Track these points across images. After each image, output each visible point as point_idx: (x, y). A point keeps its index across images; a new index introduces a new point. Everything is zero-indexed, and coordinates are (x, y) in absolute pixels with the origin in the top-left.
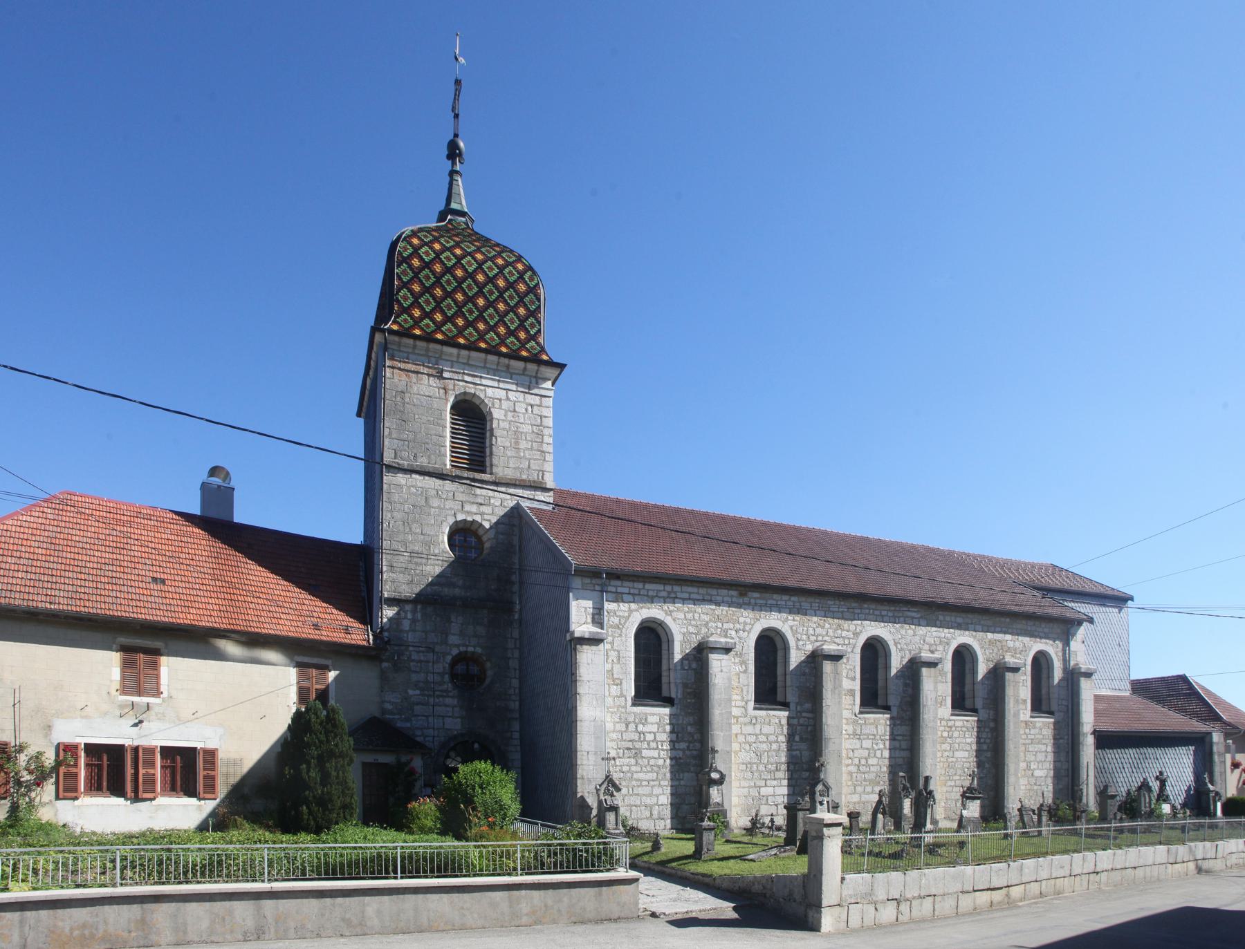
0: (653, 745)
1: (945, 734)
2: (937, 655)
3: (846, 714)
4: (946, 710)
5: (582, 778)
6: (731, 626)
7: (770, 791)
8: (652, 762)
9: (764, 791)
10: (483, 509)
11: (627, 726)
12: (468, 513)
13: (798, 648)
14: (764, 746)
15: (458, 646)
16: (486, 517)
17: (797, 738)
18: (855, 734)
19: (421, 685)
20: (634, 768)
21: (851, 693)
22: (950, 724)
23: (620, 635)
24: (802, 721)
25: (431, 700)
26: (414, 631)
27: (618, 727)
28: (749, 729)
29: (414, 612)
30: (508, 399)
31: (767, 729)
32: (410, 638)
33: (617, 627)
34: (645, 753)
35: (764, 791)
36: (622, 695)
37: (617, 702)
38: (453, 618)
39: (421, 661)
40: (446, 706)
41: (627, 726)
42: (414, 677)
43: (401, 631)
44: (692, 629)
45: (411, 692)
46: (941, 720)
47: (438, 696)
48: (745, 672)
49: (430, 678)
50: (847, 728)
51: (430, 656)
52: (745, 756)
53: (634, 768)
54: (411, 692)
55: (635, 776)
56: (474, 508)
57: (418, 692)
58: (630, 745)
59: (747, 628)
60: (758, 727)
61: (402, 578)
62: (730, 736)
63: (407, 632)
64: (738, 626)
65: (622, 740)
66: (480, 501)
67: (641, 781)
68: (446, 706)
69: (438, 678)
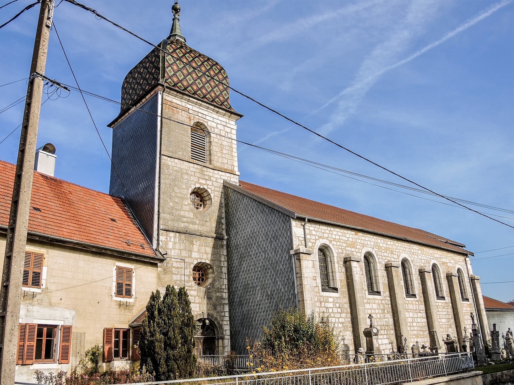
12: (201, 184)
15: (197, 259)
17: (386, 312)
26: (175, 249)
29: (175, 237)
38: (194, 242)
43: (168, 249)
56: (203, 182)
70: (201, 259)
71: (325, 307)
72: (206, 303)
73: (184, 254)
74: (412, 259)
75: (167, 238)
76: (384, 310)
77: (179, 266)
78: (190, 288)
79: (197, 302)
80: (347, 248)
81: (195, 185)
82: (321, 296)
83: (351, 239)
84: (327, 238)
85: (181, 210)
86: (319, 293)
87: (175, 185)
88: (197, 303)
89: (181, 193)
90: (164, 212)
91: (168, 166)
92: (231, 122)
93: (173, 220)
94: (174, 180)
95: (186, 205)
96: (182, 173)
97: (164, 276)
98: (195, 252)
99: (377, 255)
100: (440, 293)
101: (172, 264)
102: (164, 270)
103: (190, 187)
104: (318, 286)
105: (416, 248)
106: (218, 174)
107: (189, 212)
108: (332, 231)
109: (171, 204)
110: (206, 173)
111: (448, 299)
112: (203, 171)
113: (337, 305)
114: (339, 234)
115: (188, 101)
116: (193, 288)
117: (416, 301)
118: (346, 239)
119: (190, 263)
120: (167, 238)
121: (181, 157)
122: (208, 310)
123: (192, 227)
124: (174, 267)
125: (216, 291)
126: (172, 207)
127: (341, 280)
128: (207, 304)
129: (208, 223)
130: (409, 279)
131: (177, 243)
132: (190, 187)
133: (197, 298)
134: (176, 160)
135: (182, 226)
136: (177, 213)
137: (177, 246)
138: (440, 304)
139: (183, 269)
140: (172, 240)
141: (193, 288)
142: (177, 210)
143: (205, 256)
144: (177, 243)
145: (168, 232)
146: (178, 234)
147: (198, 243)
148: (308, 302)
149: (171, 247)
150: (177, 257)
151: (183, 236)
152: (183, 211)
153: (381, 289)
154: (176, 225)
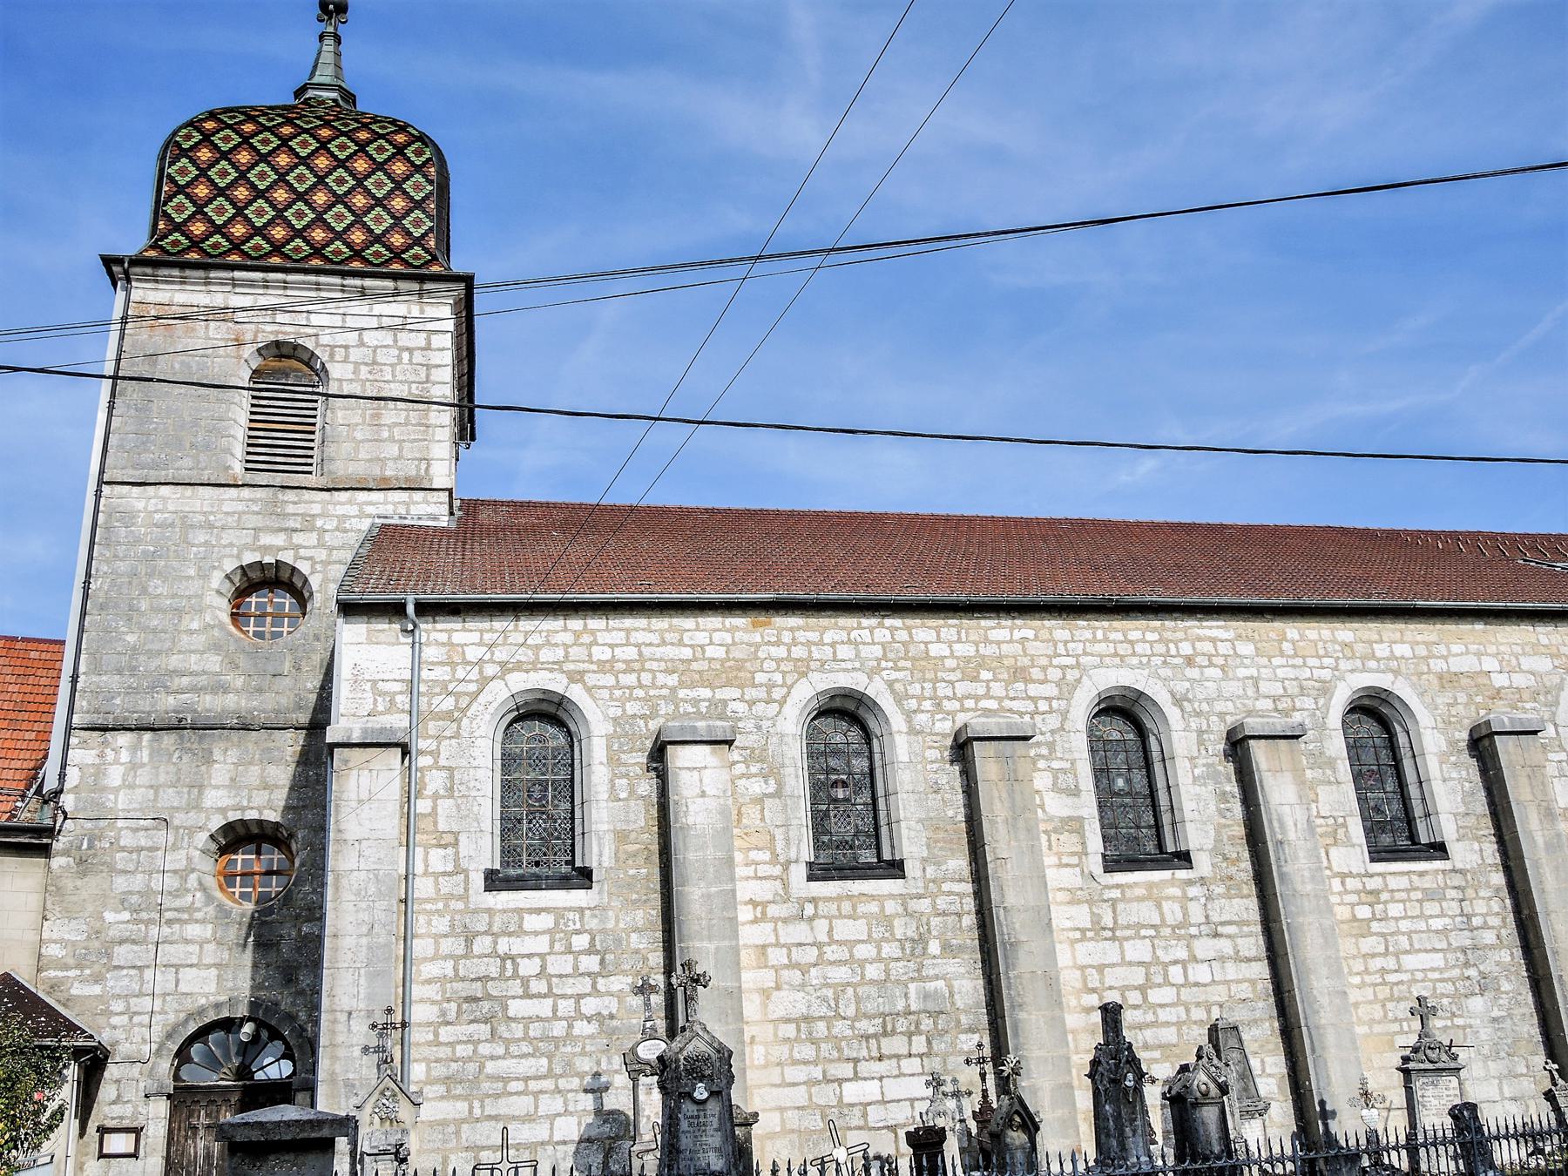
0: (538, 986)
1: (1364, 912)
2: (1297, 717)
3: (1060, 878)
4: (1352, 853)
5: (333, 1080)
6: (736, 693)
7: (871, 1090)
8: (535, 1030)
9: (852, 1092)
10: (298, 539)
11: (469, 942)
12: (266, 549)
13: (913, 731)
14: (840, 974)
15: (223, 811)
16: (302, 552)
17: (934, 947)
18: (1097, 927)
19: (134, 899)
20: (484, 1049)
21: (1073, 825)
22: (1373, 884)
23: (457, 735)
24: (942, 903)
25: (154, 931)
26: (132, 787)
27: (447, 946)
28: (799, 932)
29: (135, 748)
30: (362, 344)
31: (845, 930)
32: (122, 802)
33: (448, 716)
34: (517, 1008)
35: (852, 1092)
36: (459, 870)
37: (446, 885)
38: (217, 755)
39: (140, 849)
40: (187, 942)
41: (469, 942)
42: (121, 883)
43: (104, 789)
44: (632, 708)
45: (109, 916)
46: (1343, 876)
47: (170, 922)
48: (778, 794)
49: (156, 885)
50: (1066, 917)
51: (160, 837)
52: (790, 1002)
53: (484, 1049)
54: (109, 916)
55: (490, 1067)
56: (279, 540)
57: (126, 916)
58: (477, 989)
59: (777, 694)
60: (821, 925)
61: (112, 681)
62: (736, 951)
63: (116, 790)
64: (751, 693)
65: (457, 978)
66: (292, 524)
67: (506, 1080)
68: (187, 942)
69: (171, 882)
70: (243, 809)
71: (494, 954)
72: (249, 964)
73: (169, 798)
74: (1181, 687)
75: (101, 756)
76: (921, 940)
77: (143, 843)
78: (186, 916)
79: (207, 960)
80: (682, 693)
81: (238, 557)
82: (475, 911)
83: (711, 652)
84: (557, 666)
85: (169, 652)
86: (464, 897)
87: (150, 575)
88: (209, 966)
89: (174, 596)
90: (96, 669)
91: (128, 517)
92: (431, 312)
93: (131, 691)
94: (150, 557)
95: (191, 632)
96: (187, 526)
97: (79, 883)
98: (217, 787)
99: (899, 699)
100: (1421, 827)
101: (118, 839)
102: (81, 862)
103: (220, 568)
104: (466, 872)
105: (1215, 633)
106: (350, 502)
107: (203, 653)
108: (593, 632)
109: (131, 638)
110: (290, 509)
111: (1473, 851)
112: (275, 503)
113: (581, 942)
114: (639, 637)
115: (234, 286)
116: (199, 915)
117: (1190, 882)
118: (687, 653)
119: (192, 830)
120: (101, 756)
121: (184, 475)
122: (255, 987)
123: (210, 705)
124: (123, 849)
125: (297, 917)
126: (134, 648)
127: (621, 837)
128: (255, 966)
129: (287, 681)
130: (1160, 784)
131: (143, 765)
132: (220, 568)
133: (211, 947)
134: (164, 490)
135: (167, 704)
136: (154, 664)
137: (144, 777)
138: (1393, 883)
139: (160, 853)
140: (125, 756)
141: (199, 915)
142: (151, 654)
143: (260, 798)
144: (143, 765)
145: (108, 735)
146: (147, 736)
147: (233, 755)
148: (348, 942)
149: (117, 783)
150: (139, 815)
151: (169, 739)
152: (180, 652)
153: (1448, 830)
154: (144, 704)
